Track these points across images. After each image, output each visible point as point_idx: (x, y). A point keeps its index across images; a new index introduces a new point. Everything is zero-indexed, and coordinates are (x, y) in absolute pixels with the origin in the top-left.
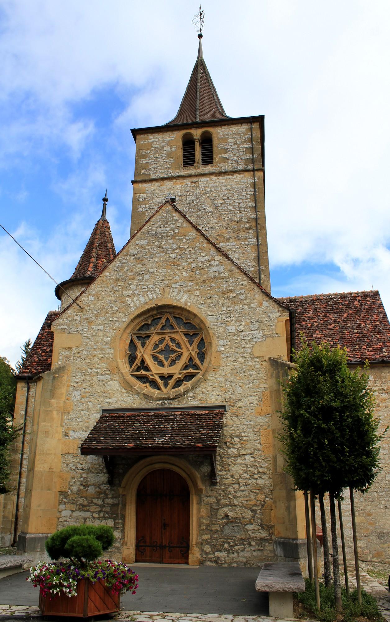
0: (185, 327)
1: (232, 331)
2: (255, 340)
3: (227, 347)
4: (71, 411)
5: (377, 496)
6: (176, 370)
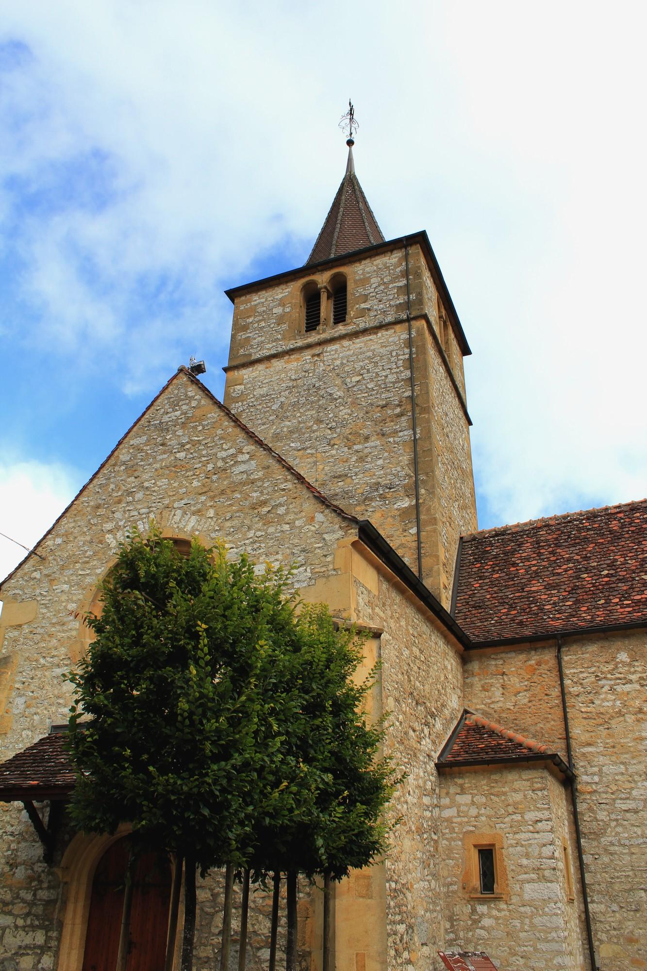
4: (9, 732)
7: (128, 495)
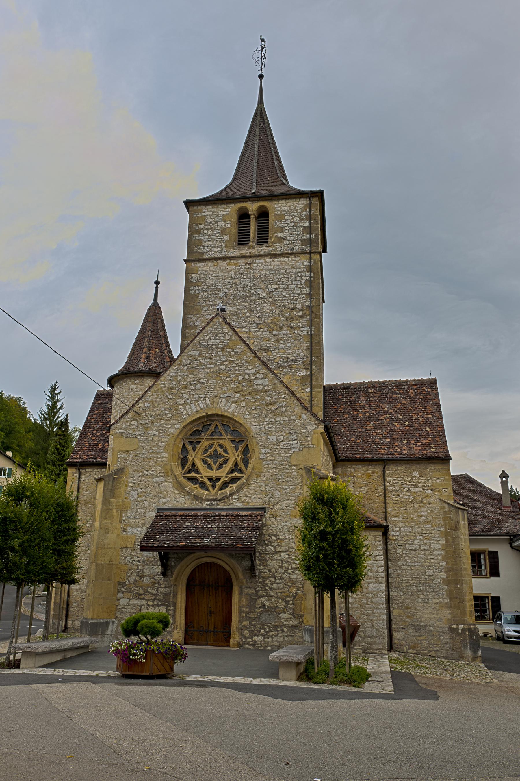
0: (231, 434)
1: (273, 441)
2: (293, 450)
3: (268, 455)
5: (416, 590)
6: (223, 473)
7: (191, 384)
